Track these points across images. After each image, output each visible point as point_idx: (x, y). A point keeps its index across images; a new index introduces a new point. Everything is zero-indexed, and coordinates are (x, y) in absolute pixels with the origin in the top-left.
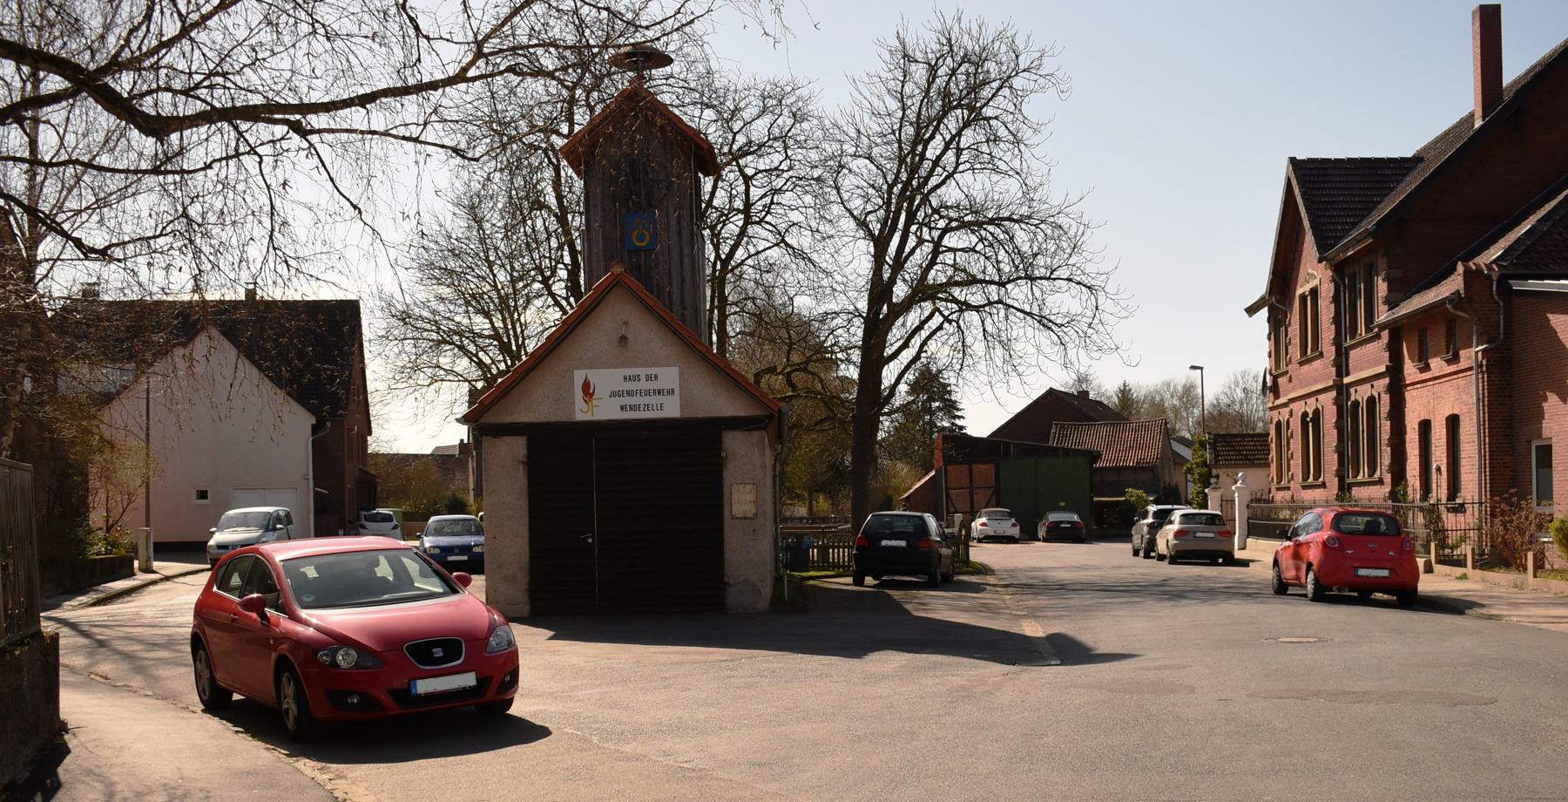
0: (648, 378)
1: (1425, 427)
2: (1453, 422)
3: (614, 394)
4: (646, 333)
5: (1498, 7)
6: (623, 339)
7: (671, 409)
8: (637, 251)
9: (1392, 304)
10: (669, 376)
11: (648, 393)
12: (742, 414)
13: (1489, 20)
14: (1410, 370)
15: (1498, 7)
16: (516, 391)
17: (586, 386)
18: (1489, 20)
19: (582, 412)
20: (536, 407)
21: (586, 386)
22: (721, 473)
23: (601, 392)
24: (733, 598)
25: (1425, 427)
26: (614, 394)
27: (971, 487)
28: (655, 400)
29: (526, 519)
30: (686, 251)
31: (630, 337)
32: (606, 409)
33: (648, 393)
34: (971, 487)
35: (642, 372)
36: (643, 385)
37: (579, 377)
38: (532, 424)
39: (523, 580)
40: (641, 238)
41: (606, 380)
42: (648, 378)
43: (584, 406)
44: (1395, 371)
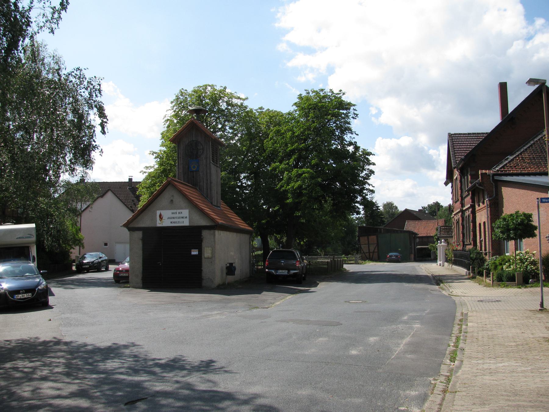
0: (179, 213)
1: (480, 224)
2: (484, 223)
3: (169, 218)
4: (178, 199)
5: (506, 83)
6: (172, 201)
7: (186, 223)
8: (193, 172)
9: (471, 183)
10: (186, 212)
11: (179, 218)
12: (208, 224)
13: (503, 87)
14: (477, 208)
15: (506, 83)
16: (139, 218)
17: (160, 215)
18: (503, 87)
19: (159, 224)
20: (145, 222)
21: (160, 215)
22: (201, 243)
23: (165, 217)
24: (204, 283)
25: (480, 224)
26: (169, 218)
27: (369, 244)
28: (181, 220)
29: (142, 257)
30: (208, 171)
31: (174, 200)
32: (166, 223)
33: (179, 218)
34: (369, 244)
35: (178, 211)
36: (178, 215)
37: (158, 213)
38: (144, 228)
39: (140, 276)
40: (194, 167)
41: (166, 214)
42: (179, 213)
43: (160, 222)
44: (473, 207)
